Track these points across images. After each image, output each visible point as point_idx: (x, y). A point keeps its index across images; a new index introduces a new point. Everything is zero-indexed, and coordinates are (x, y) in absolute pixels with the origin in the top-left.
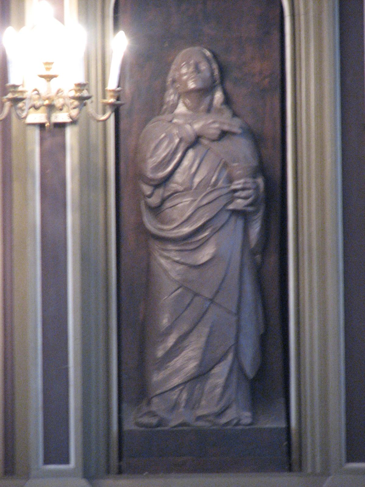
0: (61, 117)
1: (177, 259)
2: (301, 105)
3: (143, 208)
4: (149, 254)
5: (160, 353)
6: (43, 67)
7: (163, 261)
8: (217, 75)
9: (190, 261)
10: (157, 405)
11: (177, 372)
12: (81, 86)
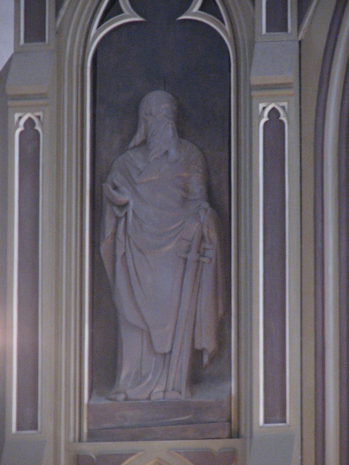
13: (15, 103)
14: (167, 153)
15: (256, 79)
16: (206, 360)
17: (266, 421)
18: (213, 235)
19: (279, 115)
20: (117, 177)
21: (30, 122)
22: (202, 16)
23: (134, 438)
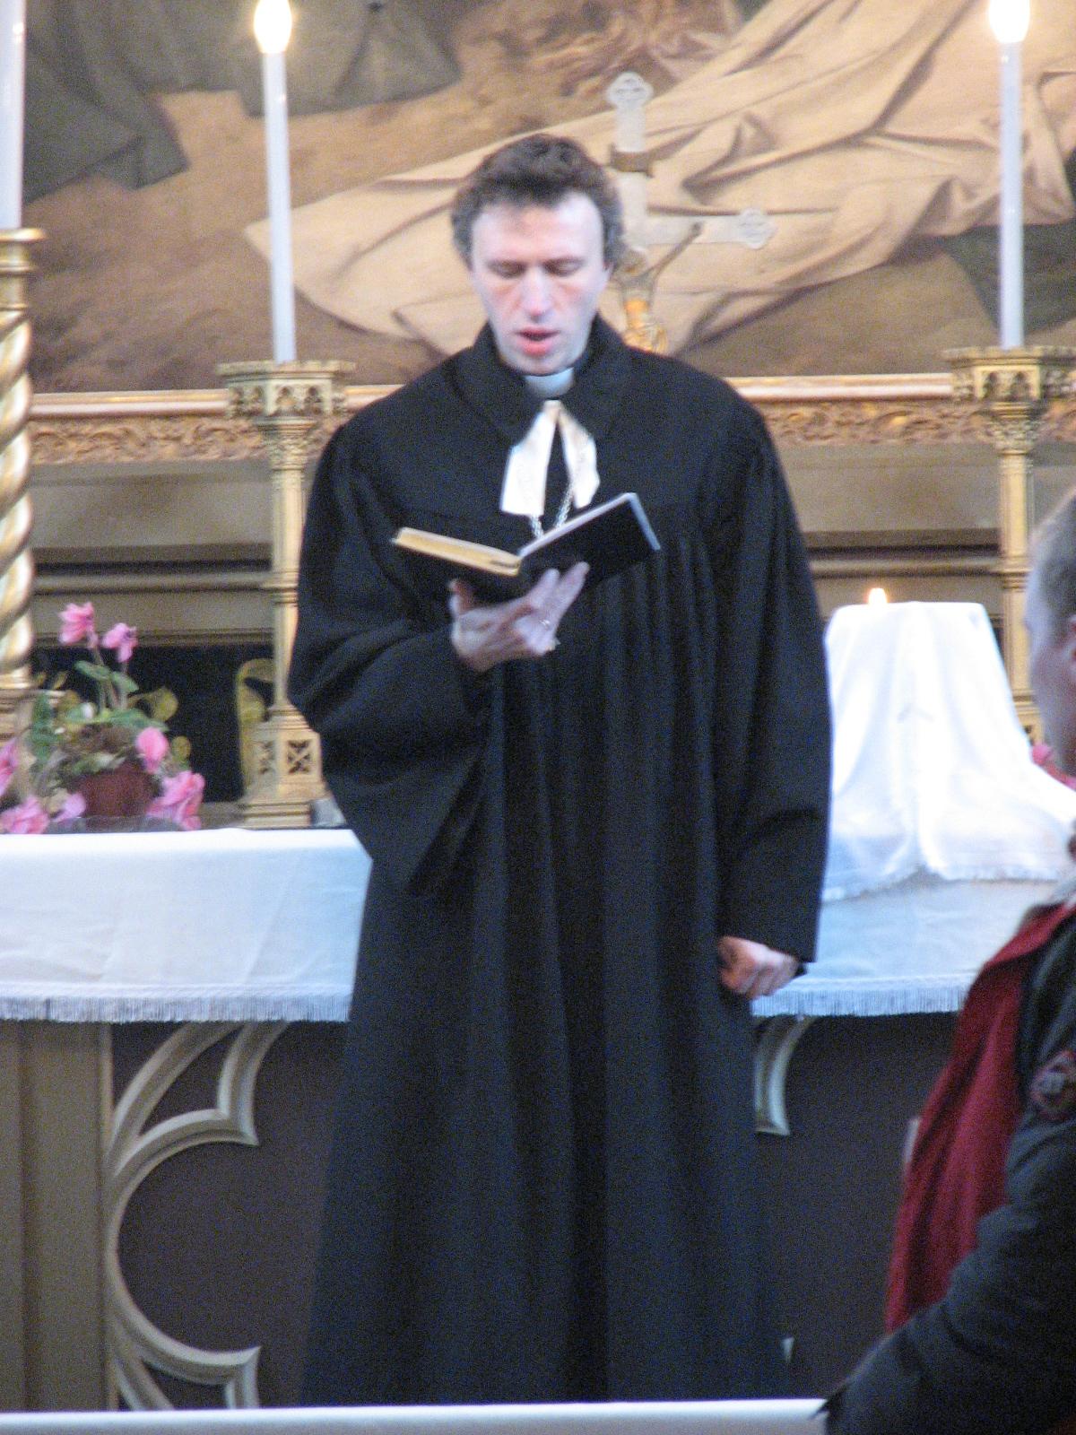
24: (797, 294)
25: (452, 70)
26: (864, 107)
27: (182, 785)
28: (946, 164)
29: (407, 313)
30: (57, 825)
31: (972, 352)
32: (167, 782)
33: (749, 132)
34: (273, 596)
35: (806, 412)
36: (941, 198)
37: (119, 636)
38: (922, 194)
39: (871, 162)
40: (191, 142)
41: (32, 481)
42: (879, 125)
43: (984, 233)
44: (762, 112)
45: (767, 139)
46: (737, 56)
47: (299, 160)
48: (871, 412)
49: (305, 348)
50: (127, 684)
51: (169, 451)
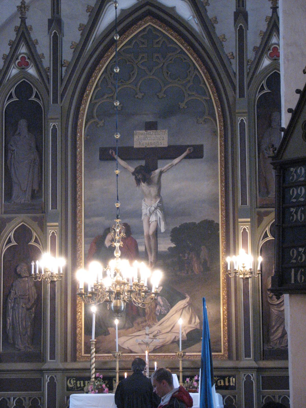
0: (248, 276)
1: (276, 309)
2: (103, 11)
3: (268, 297)
4: (269, 308)
5: (272, 332)
6: (242, 265)
7: (273, 310)
8: (78, 297)
9: (279, 310)
10: (271, 344)
11: (276, 336)
12: (251, 269)
13: (239, 115)
14: (25, 136)
15: (49, 117)
16: (36, 192)
17: (52, 209)
18: (38, 159)
19: (56, 126)
20: (12, 143)
21: (54, 126)
22: (35, 99)
23: (16, 213)
24: (163, 346)
25: (133, 326)
26: (169, 329)
27: (106, 389)
28: (176, 334)
29: (129, 347)
30: (95, 393)
31: (177, 351)
32: (105, 389)
33: (159, 331)
34: (179, 372)
35: (163, 356)
36: (176, 337)
37: (101, 376)
38: (174, 337)
39: (169, 334)
40: (110, 332)
41: (95, 362)
42: (170, 331)
43: (179, 341)
44: (160, 330)
45: (160, 332)
46: (158, 325)
47: (119, 334)
48: (169, 356)
49: (119, 350)
50: (102, 380)
51: (108, 359)
